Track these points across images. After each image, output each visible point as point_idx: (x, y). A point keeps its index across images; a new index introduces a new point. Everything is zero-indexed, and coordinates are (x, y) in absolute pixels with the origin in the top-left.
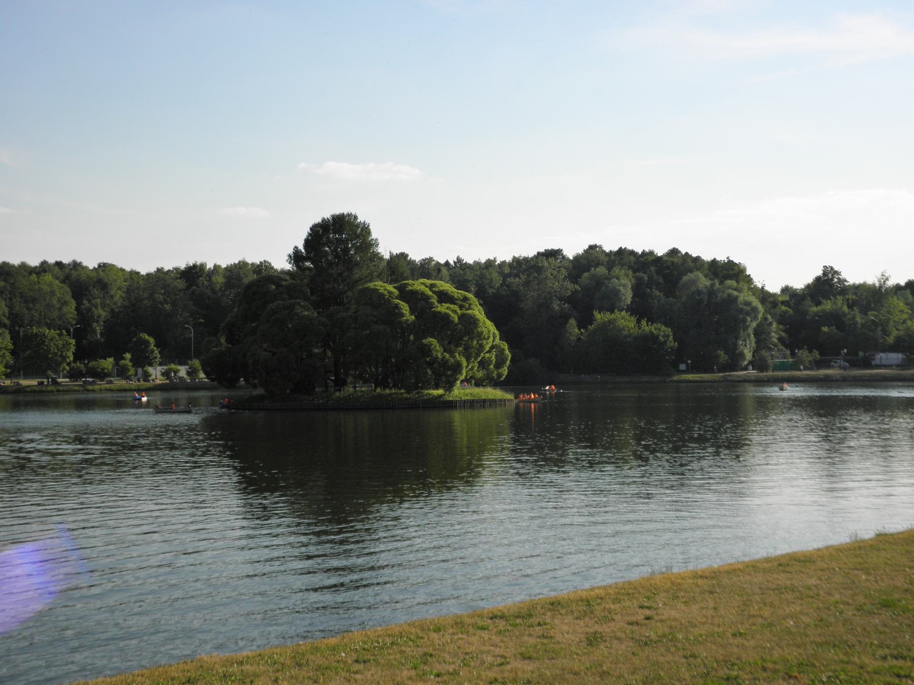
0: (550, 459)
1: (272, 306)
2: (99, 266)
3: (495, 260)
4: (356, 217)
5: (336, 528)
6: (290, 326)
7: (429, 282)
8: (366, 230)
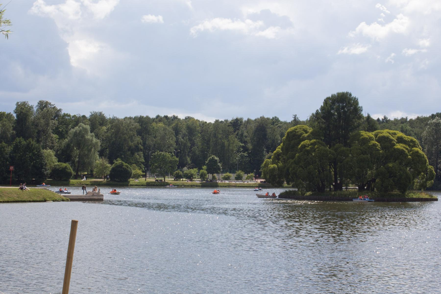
0: (337, 216)
1: (302, 143)
2: (186, 118)
3: (407, 119)
4: (350, 95)
5: (39, 190)
6: (313, 154)
7: (391, 131)
8: (356, 101)
